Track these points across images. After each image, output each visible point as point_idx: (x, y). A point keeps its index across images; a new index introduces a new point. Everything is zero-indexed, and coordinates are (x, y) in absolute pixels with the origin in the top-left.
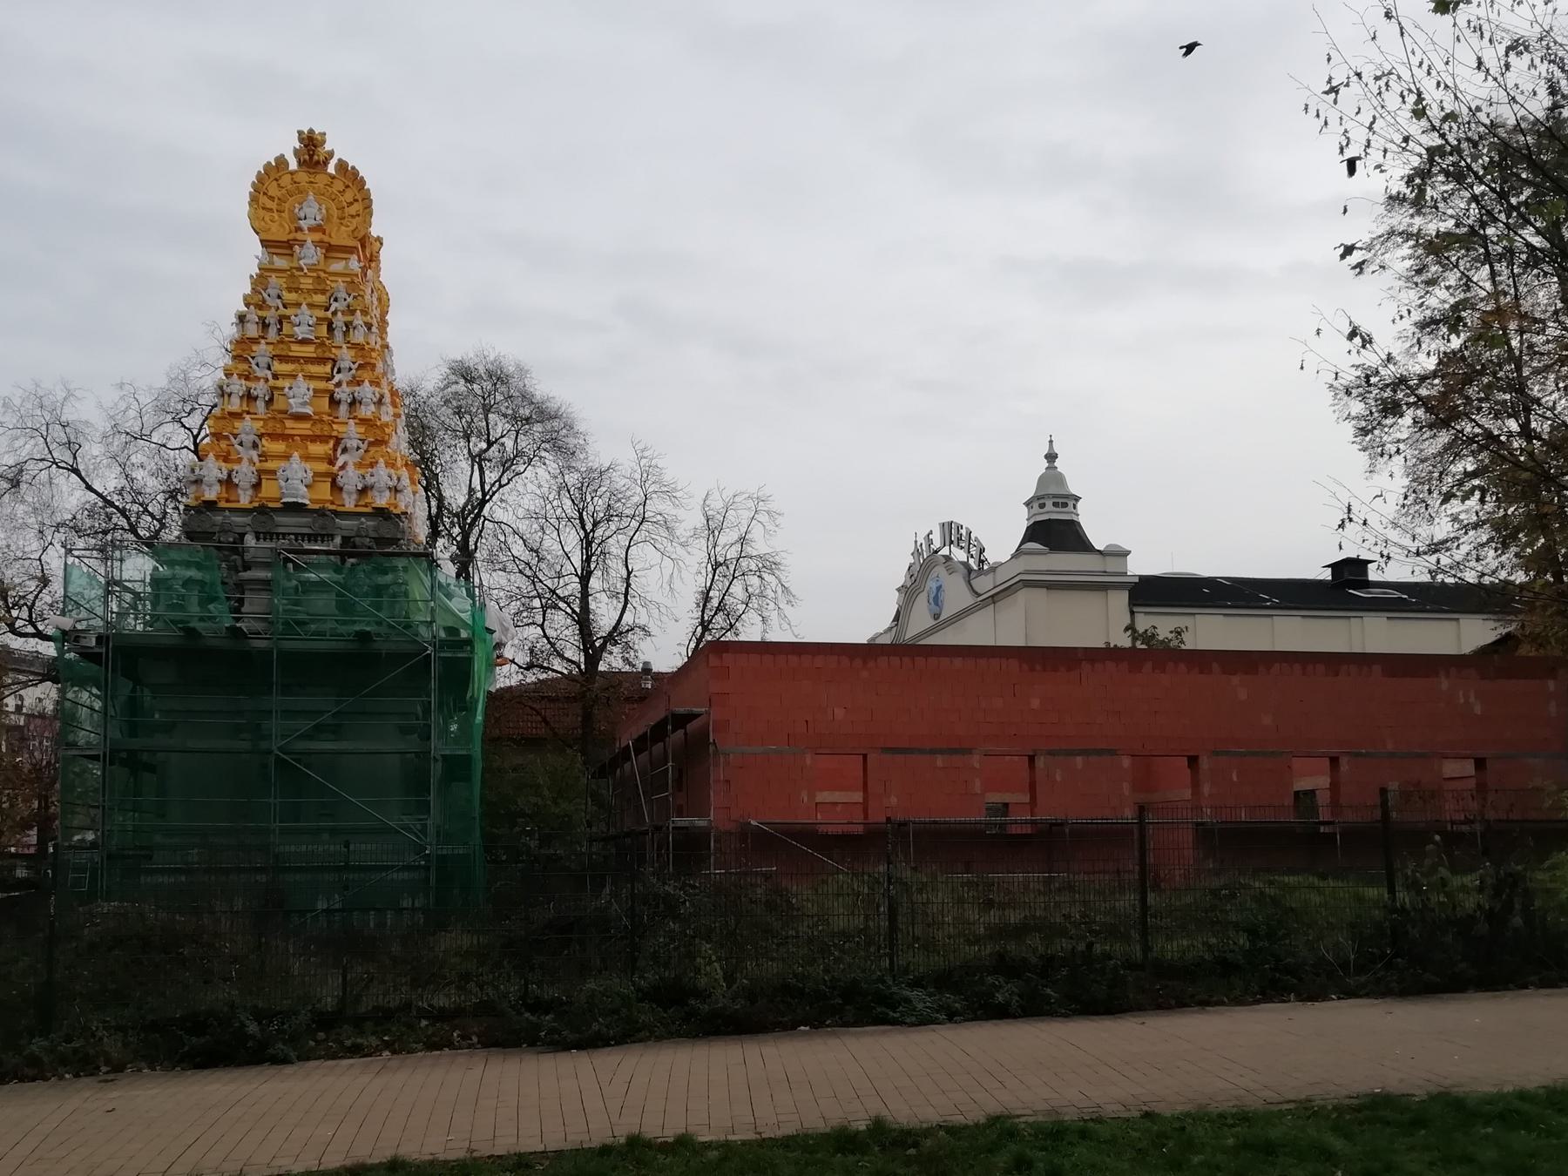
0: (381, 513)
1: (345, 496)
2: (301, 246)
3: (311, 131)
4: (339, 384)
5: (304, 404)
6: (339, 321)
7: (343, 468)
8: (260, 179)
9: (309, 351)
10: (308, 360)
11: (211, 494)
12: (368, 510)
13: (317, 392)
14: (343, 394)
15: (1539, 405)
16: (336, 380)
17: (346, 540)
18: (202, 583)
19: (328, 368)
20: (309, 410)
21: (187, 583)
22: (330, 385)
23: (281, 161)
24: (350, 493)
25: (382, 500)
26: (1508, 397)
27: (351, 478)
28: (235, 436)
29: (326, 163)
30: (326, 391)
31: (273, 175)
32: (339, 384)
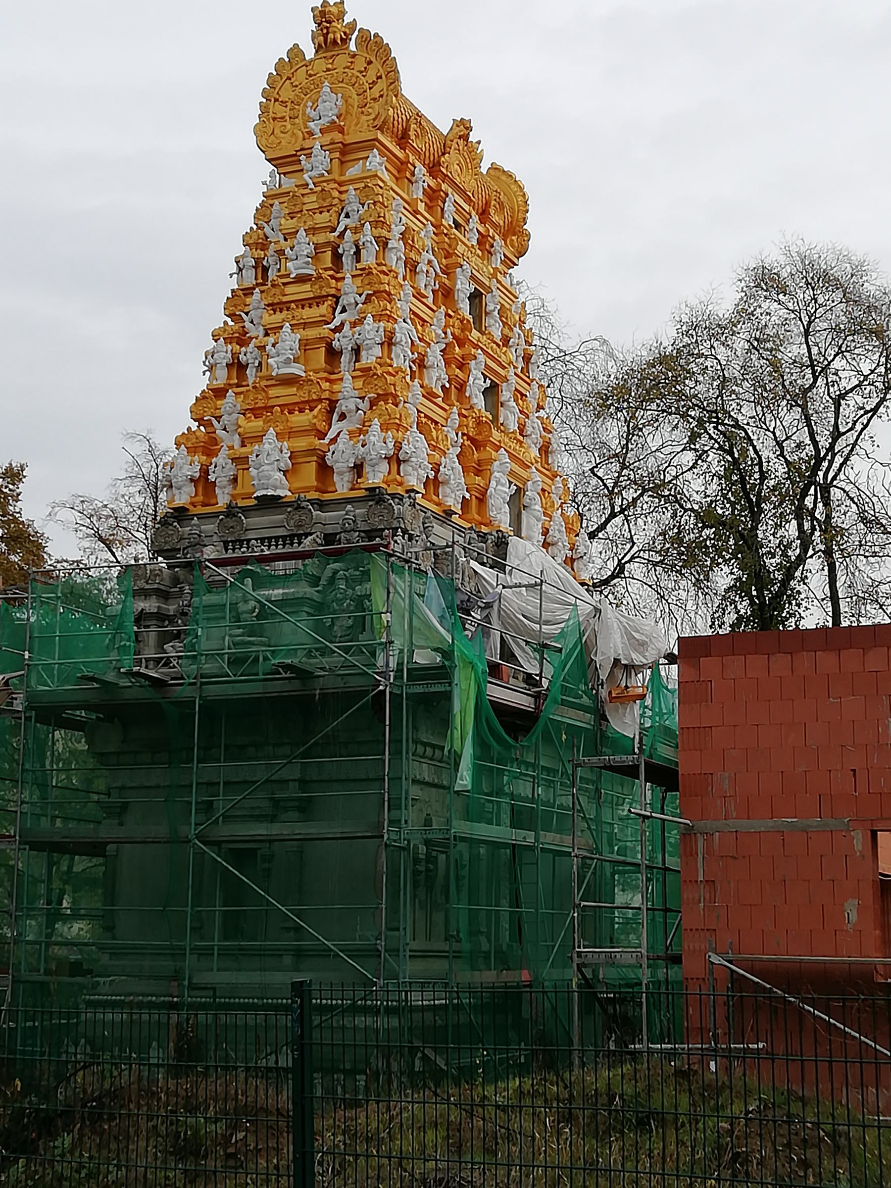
0: (375, 495)
1: (336, 478)
2: (309, 156)
4: (338, 329)
6: (347, 248)
7: (334, 441)
8: (271, 80)
9: (305, 291)
10: (302, 303)
11: (182, 499)
12: (363, 493)
13: (305, 345)
14: (342, 341)
16: (336, 322)
17: (329, 538)
19: (324, 309)
20: (297, 370)
23: (295, 52)
25: (375, 477)
27: (342, 456)
28: (218, 418)
29: (345, 41)
31: (287, 73)
32: (338, 329)
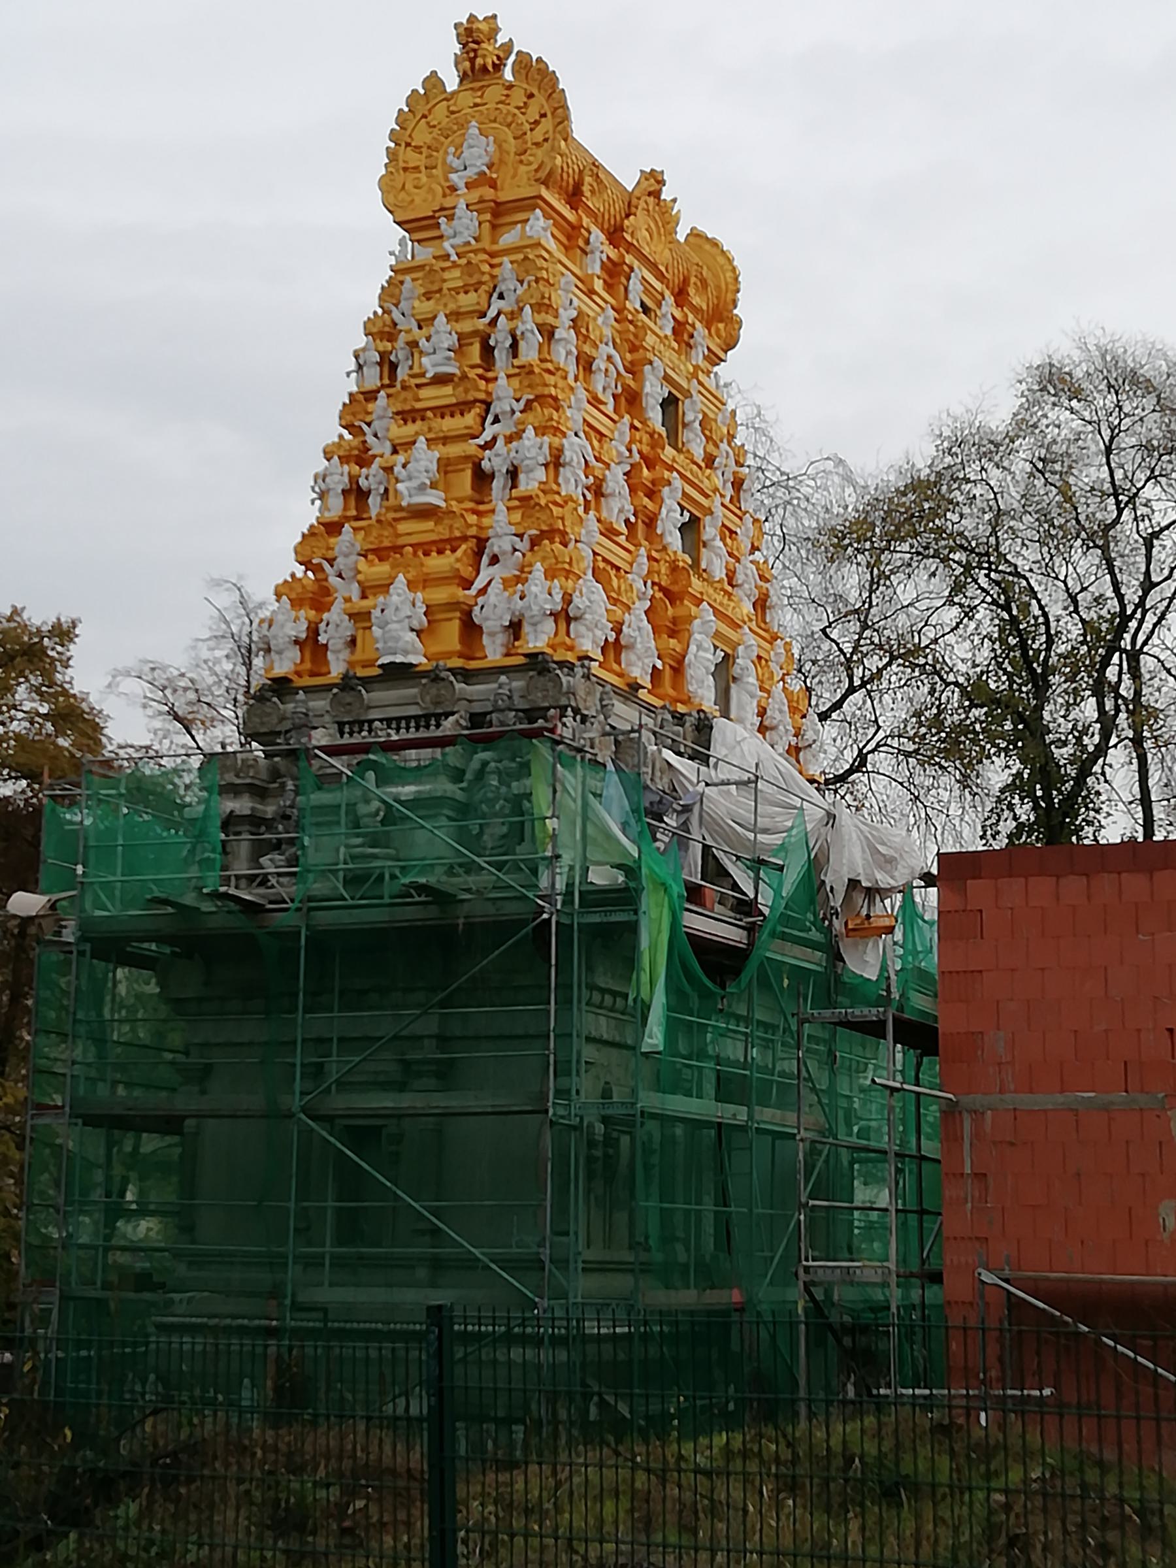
0: (537, 663)
1: (485, 640)
2: (450, 218)
3: (472, 18)
4: (490, 445)
5: (422, 488)
6: (500, 339)
7: (483, 591)
9: (445, 395)
10: (442, 411)
11: (283, 666)
13: (445, 466)
14: (494, 461)
15: (248, 687)
16: (487, 436)
17: (477, 720)
18: (255, 821)
19: (471, 418)
20: (435, 498)
21: (229, 822)
22: (471, 447)
23: (433, 81)
24: (492, 634)
25: (538, 639)
26: (882, 1391)
27: (493, 611)
28: (331, 561)
29: (498, 67)
30: (467, 458)
31: (422, 109)
32: (490, 445)
